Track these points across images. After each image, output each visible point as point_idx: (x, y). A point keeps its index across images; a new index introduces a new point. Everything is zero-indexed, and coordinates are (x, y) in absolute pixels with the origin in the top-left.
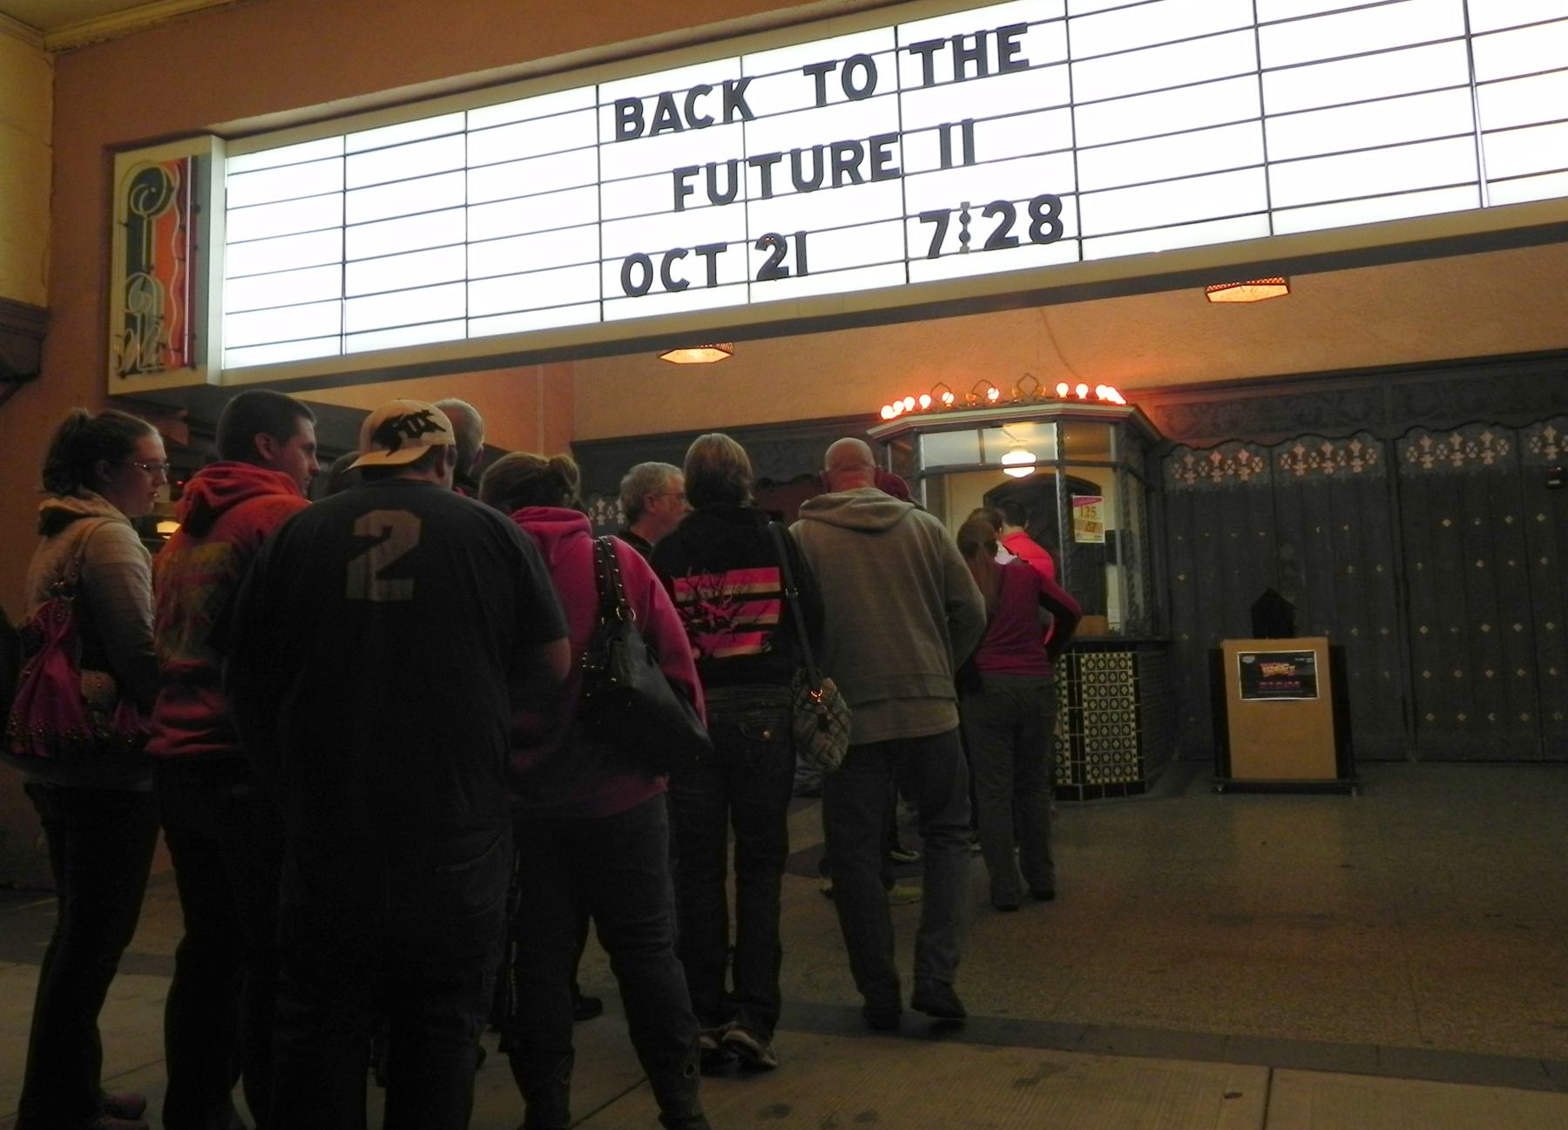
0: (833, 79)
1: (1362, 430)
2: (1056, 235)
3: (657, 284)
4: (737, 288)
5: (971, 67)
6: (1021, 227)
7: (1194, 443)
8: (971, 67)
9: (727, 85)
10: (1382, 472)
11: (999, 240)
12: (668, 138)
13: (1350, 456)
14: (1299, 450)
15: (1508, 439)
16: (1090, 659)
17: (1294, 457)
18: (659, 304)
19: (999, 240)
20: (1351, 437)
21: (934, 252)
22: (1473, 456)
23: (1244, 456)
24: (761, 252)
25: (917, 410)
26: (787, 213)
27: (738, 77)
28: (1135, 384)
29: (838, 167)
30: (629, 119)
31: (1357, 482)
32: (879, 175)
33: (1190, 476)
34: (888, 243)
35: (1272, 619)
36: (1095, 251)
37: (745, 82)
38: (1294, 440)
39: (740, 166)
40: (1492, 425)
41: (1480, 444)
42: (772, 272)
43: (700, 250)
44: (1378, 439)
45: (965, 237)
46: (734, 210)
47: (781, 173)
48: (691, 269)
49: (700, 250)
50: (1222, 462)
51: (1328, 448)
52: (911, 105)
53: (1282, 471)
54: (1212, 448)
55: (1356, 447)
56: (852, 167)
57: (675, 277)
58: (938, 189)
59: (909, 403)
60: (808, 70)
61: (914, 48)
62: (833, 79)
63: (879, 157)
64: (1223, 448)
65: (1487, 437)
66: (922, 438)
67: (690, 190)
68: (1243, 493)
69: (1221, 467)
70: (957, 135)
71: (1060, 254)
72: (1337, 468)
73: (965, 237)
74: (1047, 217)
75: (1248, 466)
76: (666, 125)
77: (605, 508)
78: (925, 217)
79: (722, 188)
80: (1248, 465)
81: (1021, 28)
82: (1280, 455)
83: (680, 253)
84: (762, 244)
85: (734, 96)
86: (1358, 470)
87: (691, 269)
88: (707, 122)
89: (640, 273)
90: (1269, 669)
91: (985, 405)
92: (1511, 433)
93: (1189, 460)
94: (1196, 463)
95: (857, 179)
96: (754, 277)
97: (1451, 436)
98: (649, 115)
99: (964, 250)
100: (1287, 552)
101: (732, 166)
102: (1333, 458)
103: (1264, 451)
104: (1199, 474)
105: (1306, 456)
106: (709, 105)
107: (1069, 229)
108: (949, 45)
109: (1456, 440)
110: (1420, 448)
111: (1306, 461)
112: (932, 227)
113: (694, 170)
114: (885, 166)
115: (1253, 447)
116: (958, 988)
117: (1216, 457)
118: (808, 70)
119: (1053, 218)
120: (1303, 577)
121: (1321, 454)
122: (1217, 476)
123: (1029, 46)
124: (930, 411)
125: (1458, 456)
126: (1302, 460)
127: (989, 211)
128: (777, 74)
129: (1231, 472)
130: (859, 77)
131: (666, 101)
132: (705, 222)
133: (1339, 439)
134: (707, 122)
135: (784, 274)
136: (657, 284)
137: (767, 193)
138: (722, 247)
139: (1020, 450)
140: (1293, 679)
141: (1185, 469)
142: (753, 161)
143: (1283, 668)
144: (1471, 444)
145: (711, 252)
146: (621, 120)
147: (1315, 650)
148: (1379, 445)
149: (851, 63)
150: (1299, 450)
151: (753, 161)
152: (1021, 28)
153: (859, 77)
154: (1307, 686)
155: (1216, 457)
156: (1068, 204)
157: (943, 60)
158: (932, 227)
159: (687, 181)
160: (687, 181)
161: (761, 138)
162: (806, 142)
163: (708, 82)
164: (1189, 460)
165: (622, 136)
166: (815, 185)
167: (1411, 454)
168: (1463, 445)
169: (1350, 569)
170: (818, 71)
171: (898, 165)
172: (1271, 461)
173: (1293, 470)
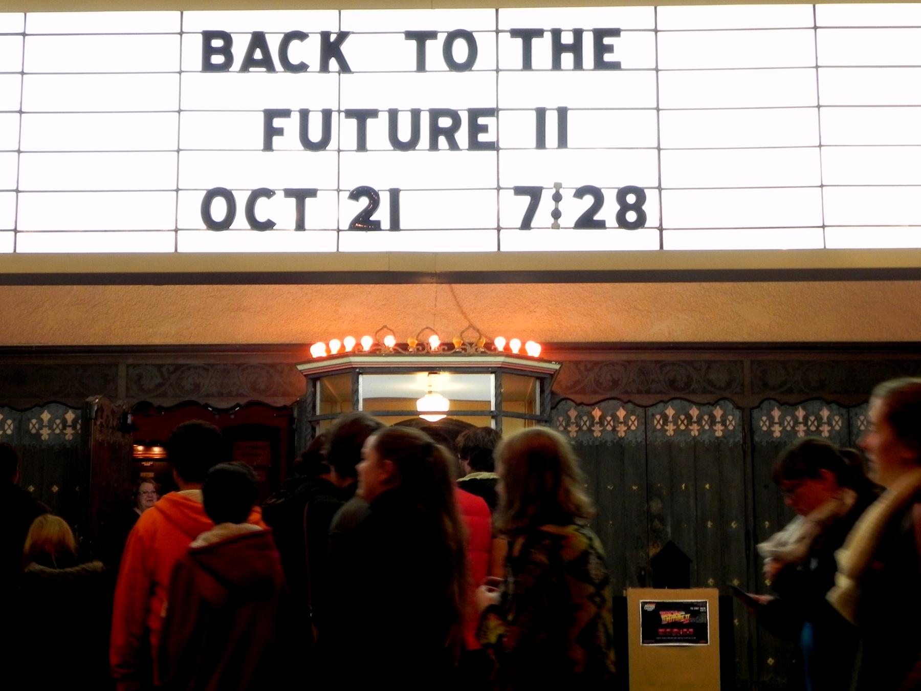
0: (434, 48)
1: (724, 399)
2: (640, 223)
3: (241, 218)
4: (326, 234)
5: (567, 59)
6: (609, 212)
7: (578, 398)
8: (567, 59)
9: (325, 35)
10: (739, 438)
11: (587, 221)
12: (258, 74)
13: (713, 421)
15: (841, 415)
17: (665, 418)
18: (240, 241)
19: (587, 221)
20: (714, 404)
21: (526, 224)
23: (621, 413)
24: (353, 202)
25: (358, 351)
26: (381, 168)
27: (337, 31)
28: (548, 339)
29: (435, 131)
30: (217, 51)
31: (718, 445)
32: (475, 145)
34: (482, 211)
35: (671, 570)
36: (673, 243)
37: (343, 36)
38: (666, 402)
39: (334, 116)
40: (828, 403)
41: (819, 419)
42: (364, 222)
43: (289, 193)
44: (738, 408)
45: (556, 214)
46: (326, 157)
47: (377, 129)
48: (277, 209)
49: (289, 193)
50: (602, 418)
51: (694, 412)
52: (511, 87)
53: (655, 430)
54: (593, 405)
55: (718, 412)
56: (450, 134)
57: (261, 217)
58: (526, 164)
59: (350, 343)
60: (410, 35)
61: (515, 33)
62: (434, 48)
63: (475, 129)
64: (603, 404)
65: (825, 413)
66: (361, 378)
67: (280, 132)
68: (619, 448)
69: (601, 423)
70: (552, 120)
71: (641, 241)
72: (702, 431)
73: (556, 214)
74: (633, 206)
75: (623, 423)
76: (258, 63)
78: (520, 191)
79: (315, 135)
80: (625, 423)
81: (615, 32)
82: (653, 415)
83: (268, 193)
84: (356, 195)
85: (331, 48)
86: (719, 434)
87: (277, 209)
88: (302, 68)
89: (219, 206)
90: (667, 617)
91: (423, 348)
92: (844, 411)
93: (573, 413)
94: (579, 417)
95: (453, 146)
96: (345, 225)
97: (796, 409)
98: (239, 50)
99: (556, 226)
100: (656, 506)
101: (327, 115)
102: (699, 422)
103: (640, 411)
104: (580, 429)
105: (676, 417)
106: (306, 51)
107: (652, 220)
108: (548, 36)
109: (800, 413)
110: (771, 418)
111: (675, 423)
112: (526, 200)
113: (286, 113)
114: (482, 137)
115: (630, 406)
117: (597, 413)
118: (410, 35)
119: (638, 207)
120: (669, 529)
121: (689, 417)
122: (597, 431)
123: (621, 49)
124: (353, 354)
126: (674, 422)
127: (580, 193)
128: (375, 37)
129: (609, 428)
130: (460, 50)
131: (258, 40)
132: (290, 164)
133: (704, 405)
134: (302, 68)
135: (376, 226)
136: (241, 218)
137: (362, 145)
138: (312, 193)
139: (434, 396)
140: (688, 626)
142: (350, 114)
143: (679, 616)
145: (301, 196)
146: (208, 51)
147: (707, 598)
149: (453, 36)
150: (670, 412)
151: (350, 114)
152: (615, 32)
153: (460, 50)
154: (699, 634)
155: (597, 413)
156: (651, 197)
157: (542, 48)
158: (526, 200)
159: (277, 123)
160: (277, 123)
161: (356, 92)
162: (405, 106)
163: (305, 30)
164: (573, 413)
165: (208, 67)
166: (411, 145)
168: (806, 418)
169: (709, 524)
170: (421, 38)
171: (494, 139)
172: (646, 422)
173: (664, 431)
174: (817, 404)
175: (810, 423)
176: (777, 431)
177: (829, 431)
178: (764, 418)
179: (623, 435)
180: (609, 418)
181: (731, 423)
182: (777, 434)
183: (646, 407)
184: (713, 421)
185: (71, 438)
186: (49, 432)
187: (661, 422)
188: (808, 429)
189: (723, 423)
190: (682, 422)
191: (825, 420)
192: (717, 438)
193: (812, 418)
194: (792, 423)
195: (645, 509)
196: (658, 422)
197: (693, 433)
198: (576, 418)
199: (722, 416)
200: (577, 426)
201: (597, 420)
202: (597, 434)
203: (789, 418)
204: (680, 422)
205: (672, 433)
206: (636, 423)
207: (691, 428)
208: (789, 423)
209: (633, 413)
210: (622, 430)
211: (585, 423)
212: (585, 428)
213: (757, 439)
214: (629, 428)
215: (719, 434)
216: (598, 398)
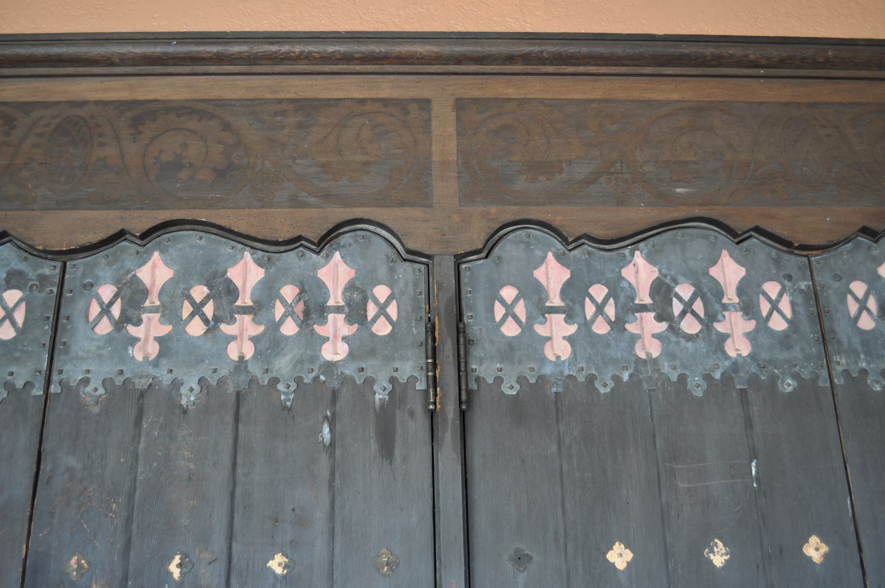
10: (410, 367)
51: (247, 273)
55: (335, 272)
72: (270, 343)
77: (574, 292)
92: (792, 262)
97: (624, 261)
109: (640, 272)
116: (319, 276)
125: (647, 327)
144: (599, 292)
148: (407, 272)
164: (553, 275)
167: (503, 314)
174: (696, 243)
175: (677, 307)
176: (558, 338)
177: (751, 336)
178: (509, 293)
181: (382, 310)
182: (559, 349)
183: (64, 256)
184: (313, 310)
185: (745, 350)
187: (116, 311)
188: (674, 329)
189: (355, 311)
191: (731, 296)
192: (329, 367)
193: (685, 291)
194: (610, 310)
196: (106, 310)
197: (233, 353)
199: (351, 287)
201: (336, 298)
204: (187, 309)
205: (153, 349)
208: (600, 309)
210: (335, 342)
213: (484, 368)
215: (739, 347)
216: (639, 214)
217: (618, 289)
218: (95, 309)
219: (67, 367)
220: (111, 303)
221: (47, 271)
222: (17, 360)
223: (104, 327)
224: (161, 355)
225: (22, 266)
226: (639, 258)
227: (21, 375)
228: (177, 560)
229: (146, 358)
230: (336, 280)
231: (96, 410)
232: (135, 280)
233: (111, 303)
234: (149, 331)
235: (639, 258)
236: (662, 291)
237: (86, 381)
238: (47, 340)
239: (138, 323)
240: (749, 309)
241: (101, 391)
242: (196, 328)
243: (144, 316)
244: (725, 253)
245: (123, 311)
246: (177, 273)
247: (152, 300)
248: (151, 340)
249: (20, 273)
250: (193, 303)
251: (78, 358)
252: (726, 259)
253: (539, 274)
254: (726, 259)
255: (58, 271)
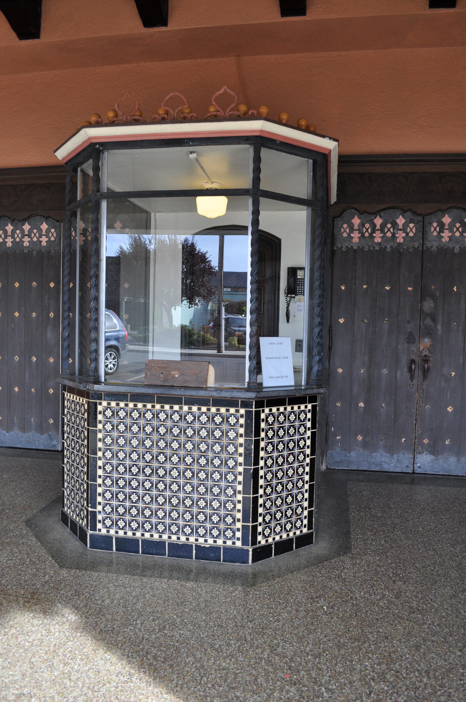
14: (447, 220)
16: (108, 407)
17: (442, 225)
20: (376, 213)
22: (35, 239)
33: (356, 236)
40: (47, 218)
65: (401, 221)
77: (13, 232)
82: (431, 224)
92: (420, 218)
97: (23, 225)
109: (26, 227)
120: (439, 327)
129: (389, 235)
141: (352, 229)
150: (447, 220)
172: (423, 231)
179: (402, 241)
180: (389, 226)
186: (29, 239)
187: (438, 229)
190: (458, 230)
195: (419, 308)
196: (435, 229)
198: (359, 225)
199: (12, 230)
200: (359, 233)
201: (378, 227)
202: (378, 240)
203: (18, 232)
204: (455, 229)
205: (447, 239)
206: (414, 230)
207: (6, 240)
209: (411, 221)
211: (367, 230)
212: (367, 235)
214: (407, 234)
217: (22, 231)
218: (432, 229)
219: (427, 243)
220: (436, 227)
221: (419, 219)
222: (415, 241)
223: (435, 234)
224: (449, 240)
225: (413, 218)
226: (27, 224)
227: (416, 245)
228: (455, 287)
229: (446, 241)
230: (27, 228)
231: (435, 253)
232: (442, 222)
233: (436, 227)
234: (446, 235)
235: (27, 224)
236: (383, 226)
237: (432, 247)
238: (421, 237)
239: (443, 232)
240: (13, 237)
241: (436, 249)
242: (457, 234)
243: (445, 231)
244: (356, 217)
245: (439, 230)
246: (452, 220)
247: (446, 227)
248: (446, 237)
249: (413, 219)
250: (456, 228)
251: (429, 241)
252: (44, 223)
253: (41, 227)
254: (44, 223)
255: (422, 219)
